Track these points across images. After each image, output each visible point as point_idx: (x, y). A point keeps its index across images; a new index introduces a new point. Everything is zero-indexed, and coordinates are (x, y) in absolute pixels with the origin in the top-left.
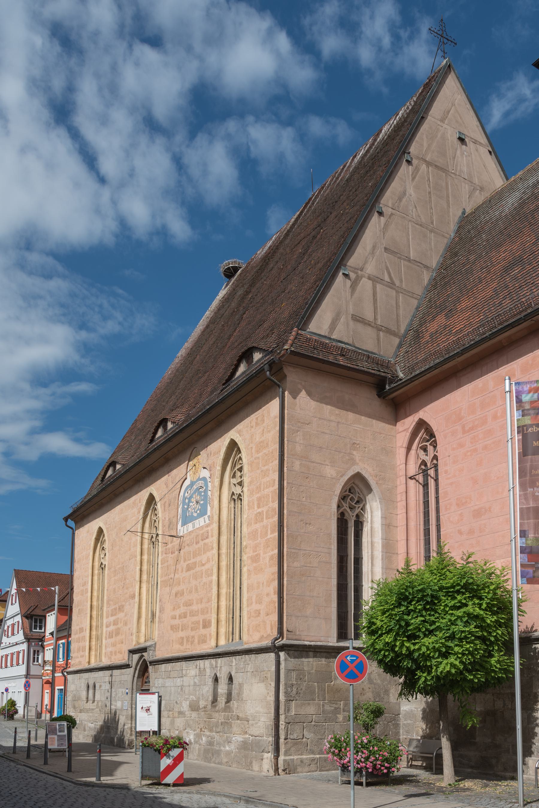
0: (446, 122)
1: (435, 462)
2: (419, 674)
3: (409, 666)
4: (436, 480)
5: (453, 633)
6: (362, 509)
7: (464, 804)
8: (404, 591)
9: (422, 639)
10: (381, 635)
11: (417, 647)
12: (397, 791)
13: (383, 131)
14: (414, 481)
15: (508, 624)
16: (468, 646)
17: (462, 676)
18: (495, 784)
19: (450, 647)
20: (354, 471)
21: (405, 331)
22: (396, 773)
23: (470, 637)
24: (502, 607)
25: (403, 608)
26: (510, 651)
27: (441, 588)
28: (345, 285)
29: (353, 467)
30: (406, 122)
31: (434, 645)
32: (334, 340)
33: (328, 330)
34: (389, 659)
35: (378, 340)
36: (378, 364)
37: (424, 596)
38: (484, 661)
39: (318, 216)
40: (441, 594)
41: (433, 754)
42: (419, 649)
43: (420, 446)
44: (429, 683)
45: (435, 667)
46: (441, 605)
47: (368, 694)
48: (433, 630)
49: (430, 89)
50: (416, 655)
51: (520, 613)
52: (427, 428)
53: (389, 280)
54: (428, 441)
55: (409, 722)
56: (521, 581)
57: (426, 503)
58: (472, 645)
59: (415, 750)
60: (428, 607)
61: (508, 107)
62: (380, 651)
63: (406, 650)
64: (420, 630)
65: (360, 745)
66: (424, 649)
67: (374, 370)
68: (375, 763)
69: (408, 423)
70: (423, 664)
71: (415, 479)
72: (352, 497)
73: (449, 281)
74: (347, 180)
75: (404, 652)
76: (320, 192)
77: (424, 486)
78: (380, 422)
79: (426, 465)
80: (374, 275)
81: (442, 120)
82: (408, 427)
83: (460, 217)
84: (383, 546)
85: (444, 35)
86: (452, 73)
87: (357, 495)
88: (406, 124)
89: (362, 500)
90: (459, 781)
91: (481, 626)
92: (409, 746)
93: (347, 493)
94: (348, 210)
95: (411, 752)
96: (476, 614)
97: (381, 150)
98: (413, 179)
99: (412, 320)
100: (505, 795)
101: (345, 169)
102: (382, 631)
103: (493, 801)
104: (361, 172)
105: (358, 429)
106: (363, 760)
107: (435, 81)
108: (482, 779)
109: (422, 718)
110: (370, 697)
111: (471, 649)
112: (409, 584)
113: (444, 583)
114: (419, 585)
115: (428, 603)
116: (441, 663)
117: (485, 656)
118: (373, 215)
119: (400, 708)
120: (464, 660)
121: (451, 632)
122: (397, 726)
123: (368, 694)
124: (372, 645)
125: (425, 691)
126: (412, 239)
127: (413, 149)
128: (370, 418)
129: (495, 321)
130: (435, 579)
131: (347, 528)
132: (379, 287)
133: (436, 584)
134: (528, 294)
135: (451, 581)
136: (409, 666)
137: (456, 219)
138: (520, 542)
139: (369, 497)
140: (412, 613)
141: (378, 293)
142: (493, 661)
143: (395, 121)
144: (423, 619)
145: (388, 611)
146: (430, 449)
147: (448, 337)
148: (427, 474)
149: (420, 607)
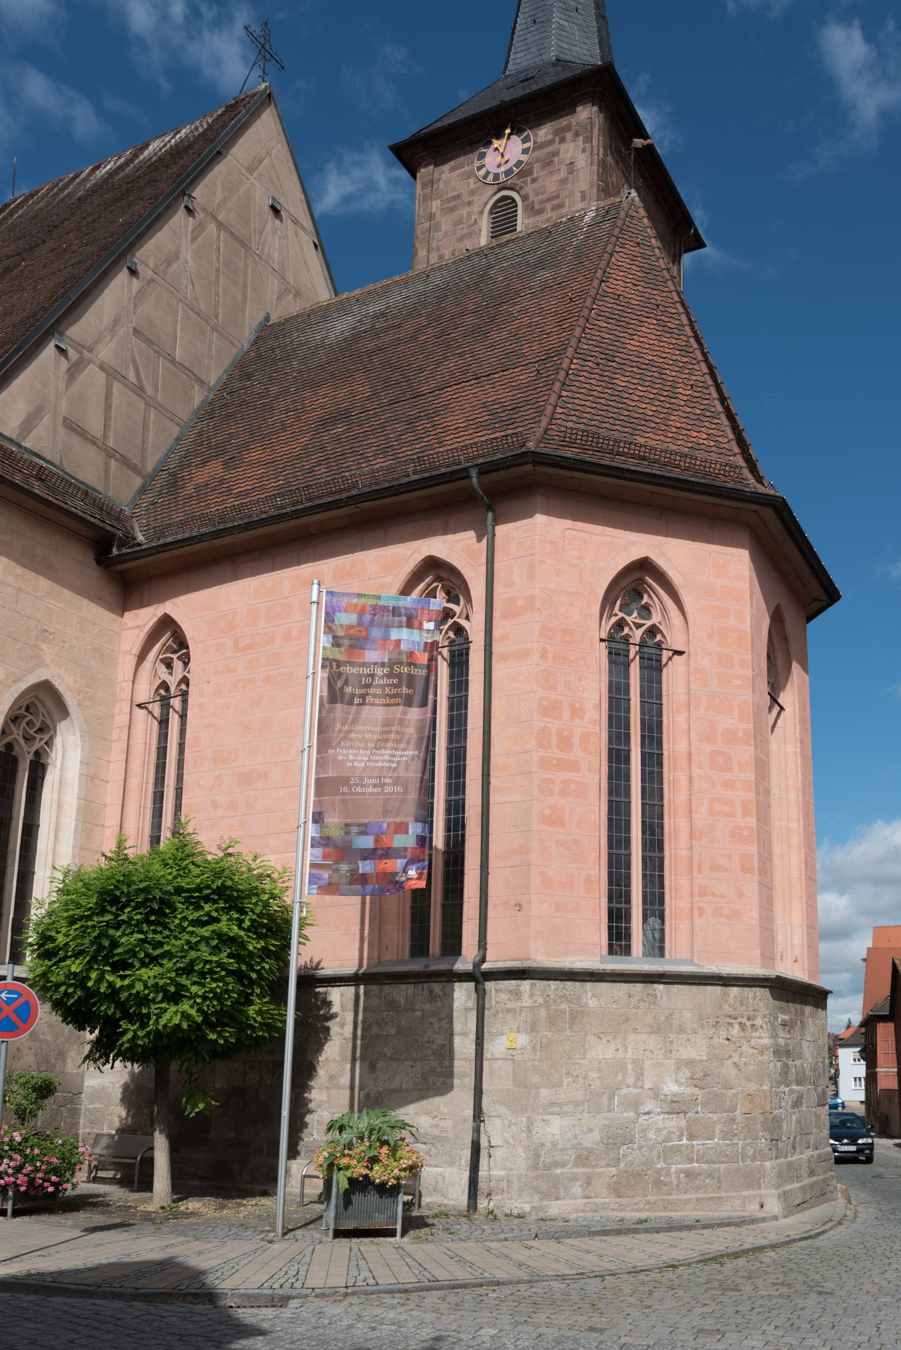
0: (255, 174)
1: (183, 687)
2: (124, 1027)
3: (110, 1013)
4: (183, 717)
5: (192, 963)
6: (46, 743)
7: (186, 1239)
8: (112, 887)
9: (137, 970)
10: (63, 960)
11: (126, 982)
12: (69, 1223)
13: (151, 147)
14: (144, 711)
15: (281, 955)
16: (214, 985)
17: (199, 1033)
18: (236, 1203)
19: (183, 986)
20: (39, 677)
21: (154, 469)
22: (69, 1192)
23: (219, 972)
24: (276, 929)
25: (108, 917)
26: (280, 998)
27: (179, 891)
28: (57, 366)
29: (38, 671)
30: (192, 149)
31: (157, 980)
32: (26, 449)
33: (18, 430)
34: (72, 1001)
35: (107, 470)
36: (102, 510)
37: (147, 900)
38: (237, 1010)
39: (19, 239)
40: (176, 898)
41: (136, 1158)
42: (131, 986)
43: (161, 657)
44: (140, 1042)
45: (154, 1017)
46: (175, 917)
47: (26, 1058)
48: (158, 956)
49: (236, 115)
50: (124, 996)
51: (301, 940)
52: (176, 632)
53: (135, 382)
54: (175, 652)
55: (97, 1105)
56: (309, 890)
57: (162, 751)
58: (221, 984)
59: (104, 1152)
60: (153, 918)
61: (350, 189)
62: (58, 986)
63: (107, 987)
64: (135, 955)
65: (8, 1145)
66: (139, 986)
67: (95, 518)
68: (32, 1176)
69: (145, 618)
70: (134, 1011)
71: (146, 708)
72: (31, 721)
73: (234, 414)
74: (79, 199)
75: (102, 990)
76: (26, 200)
77: (160, 723)
78: (94, 605)
79: (167, 689)
80: (111, 364)
81: (251, 169)
82: (143, 623)
83: (260, 323)
84: (79, 811)
85: (267, 47)
86: (273, 107)
87: (41, 718)
88: (191, 152)
89: (49, 729)
90: (178, 1202)
91: (239, 954)
92: (94, 1145)
93: (22, 711)
94: (76, 247)
95: (97, 1157)
96: (232, 935)
97: (144, 174)
98: (194, 239)
99: (167, 456)
100: (254, 1220)
101: (77, 180)
102: (67, 952)
103: (234, 1230)
104: (106, 196)
105: (55, 608)
106: (10, 1171)
107: (245, 106)
108: (216, 1196)
109: (122, 1100)
110: (31, 1064)
111: (218, 990)
112: (122, 878)
113: (183, 883)
114: (140, 882)
115: (153, 912)
116: (165, 1010)
117: (240, 1003)
118: (120, 271)
119: (83, 1082)
120: (206, 1009)
121: (187, 961)
122: (75, 1112)
123: (26, 1058)
124: (44, 975)
125: (129, 1055)
126: (181, 329)
127: (199, 192)
128: (77, 594)
129: (302, 493)
130: (170, 874)
131: (16, 771)
132: (117, 387)
133: (170, 882)
134: (354, 468)
135: (198, 881)
136: (110, 1013)
137: (255, 325)
138: (312, 831)
139: (63, 727)
140: (124, 927)
141: (114, 397)
142: (251, 1011)
143: (173, 141)
144: (142, 936)
145: (81, 918)
146: (178, 665)
147: (225, 498)
148: (169, 705)
149: (138, 917)
